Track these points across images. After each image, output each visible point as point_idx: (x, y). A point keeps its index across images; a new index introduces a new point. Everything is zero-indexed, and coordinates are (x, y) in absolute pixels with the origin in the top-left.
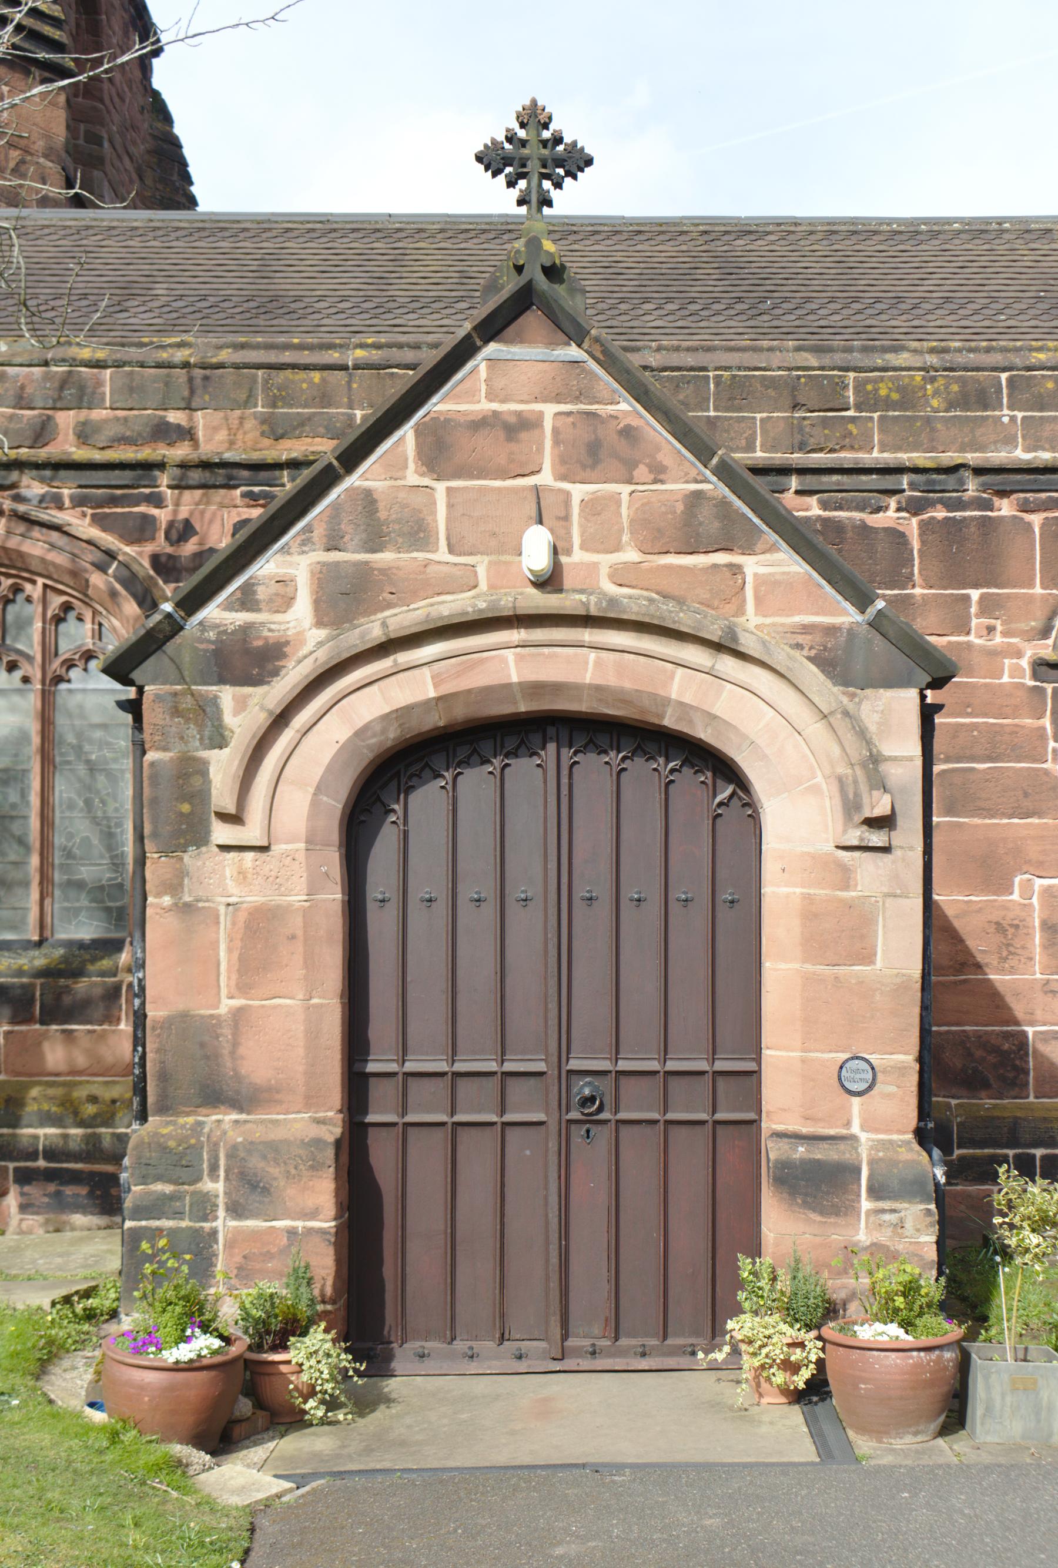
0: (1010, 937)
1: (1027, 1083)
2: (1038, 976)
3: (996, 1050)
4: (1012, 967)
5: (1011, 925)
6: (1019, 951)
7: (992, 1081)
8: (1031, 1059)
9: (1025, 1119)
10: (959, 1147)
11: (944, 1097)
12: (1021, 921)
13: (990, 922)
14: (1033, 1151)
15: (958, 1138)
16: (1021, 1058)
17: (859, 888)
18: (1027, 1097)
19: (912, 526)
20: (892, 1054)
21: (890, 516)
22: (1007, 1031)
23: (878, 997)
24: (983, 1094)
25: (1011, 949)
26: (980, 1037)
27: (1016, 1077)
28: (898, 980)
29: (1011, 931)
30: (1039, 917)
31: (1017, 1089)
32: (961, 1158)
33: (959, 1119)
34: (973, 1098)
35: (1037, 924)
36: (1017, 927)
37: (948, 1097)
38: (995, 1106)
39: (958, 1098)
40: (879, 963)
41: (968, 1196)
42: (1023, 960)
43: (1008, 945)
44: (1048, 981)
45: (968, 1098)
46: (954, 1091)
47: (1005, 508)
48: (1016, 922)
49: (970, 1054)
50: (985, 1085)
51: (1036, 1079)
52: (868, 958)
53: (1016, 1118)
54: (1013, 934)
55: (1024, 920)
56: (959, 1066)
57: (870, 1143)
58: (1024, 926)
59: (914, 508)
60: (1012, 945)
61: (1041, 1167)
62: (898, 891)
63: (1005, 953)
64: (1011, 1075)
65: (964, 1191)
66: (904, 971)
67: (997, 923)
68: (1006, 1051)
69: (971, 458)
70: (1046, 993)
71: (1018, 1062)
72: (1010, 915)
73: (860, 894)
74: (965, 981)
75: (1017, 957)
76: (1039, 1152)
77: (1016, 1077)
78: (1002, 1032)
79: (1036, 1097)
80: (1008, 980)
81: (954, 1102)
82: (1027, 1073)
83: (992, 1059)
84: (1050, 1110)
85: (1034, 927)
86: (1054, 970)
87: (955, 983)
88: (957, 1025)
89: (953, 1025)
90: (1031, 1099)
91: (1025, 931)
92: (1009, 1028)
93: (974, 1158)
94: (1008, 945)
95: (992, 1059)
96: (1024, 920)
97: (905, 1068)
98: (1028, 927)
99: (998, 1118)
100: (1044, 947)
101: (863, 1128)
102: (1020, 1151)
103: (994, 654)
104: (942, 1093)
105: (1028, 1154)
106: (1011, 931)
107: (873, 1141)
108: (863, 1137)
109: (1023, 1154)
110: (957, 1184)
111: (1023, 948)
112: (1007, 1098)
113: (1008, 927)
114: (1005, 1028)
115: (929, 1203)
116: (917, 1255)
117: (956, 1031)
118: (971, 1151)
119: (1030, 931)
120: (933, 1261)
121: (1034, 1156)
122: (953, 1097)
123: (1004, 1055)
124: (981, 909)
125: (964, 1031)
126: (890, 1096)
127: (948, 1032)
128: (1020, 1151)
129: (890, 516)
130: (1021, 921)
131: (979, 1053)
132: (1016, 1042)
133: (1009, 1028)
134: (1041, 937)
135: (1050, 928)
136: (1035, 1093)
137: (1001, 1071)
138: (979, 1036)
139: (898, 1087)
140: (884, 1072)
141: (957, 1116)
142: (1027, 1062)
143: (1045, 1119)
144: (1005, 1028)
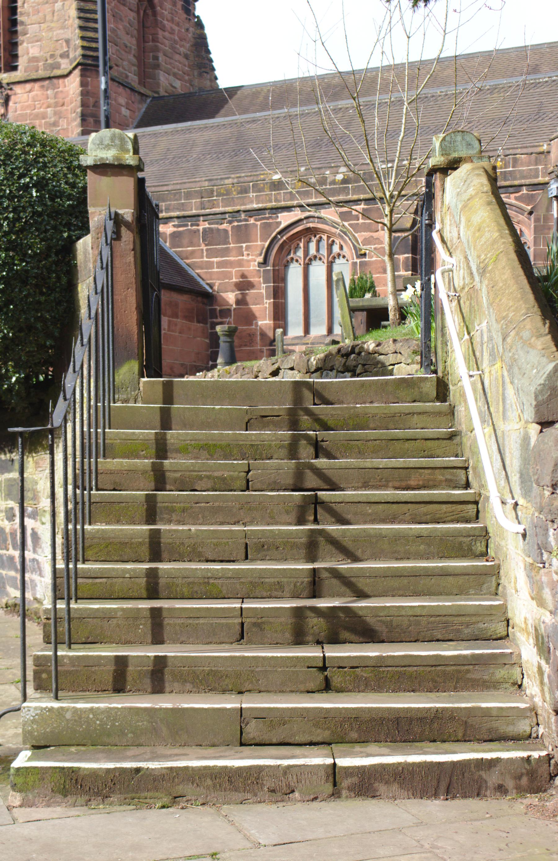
19: (229, 229)
21: (225, 226)
47: (252, 221)
59: (230, 222)
69: (243, 208)
103: (249, 261)
129: (225, 226)
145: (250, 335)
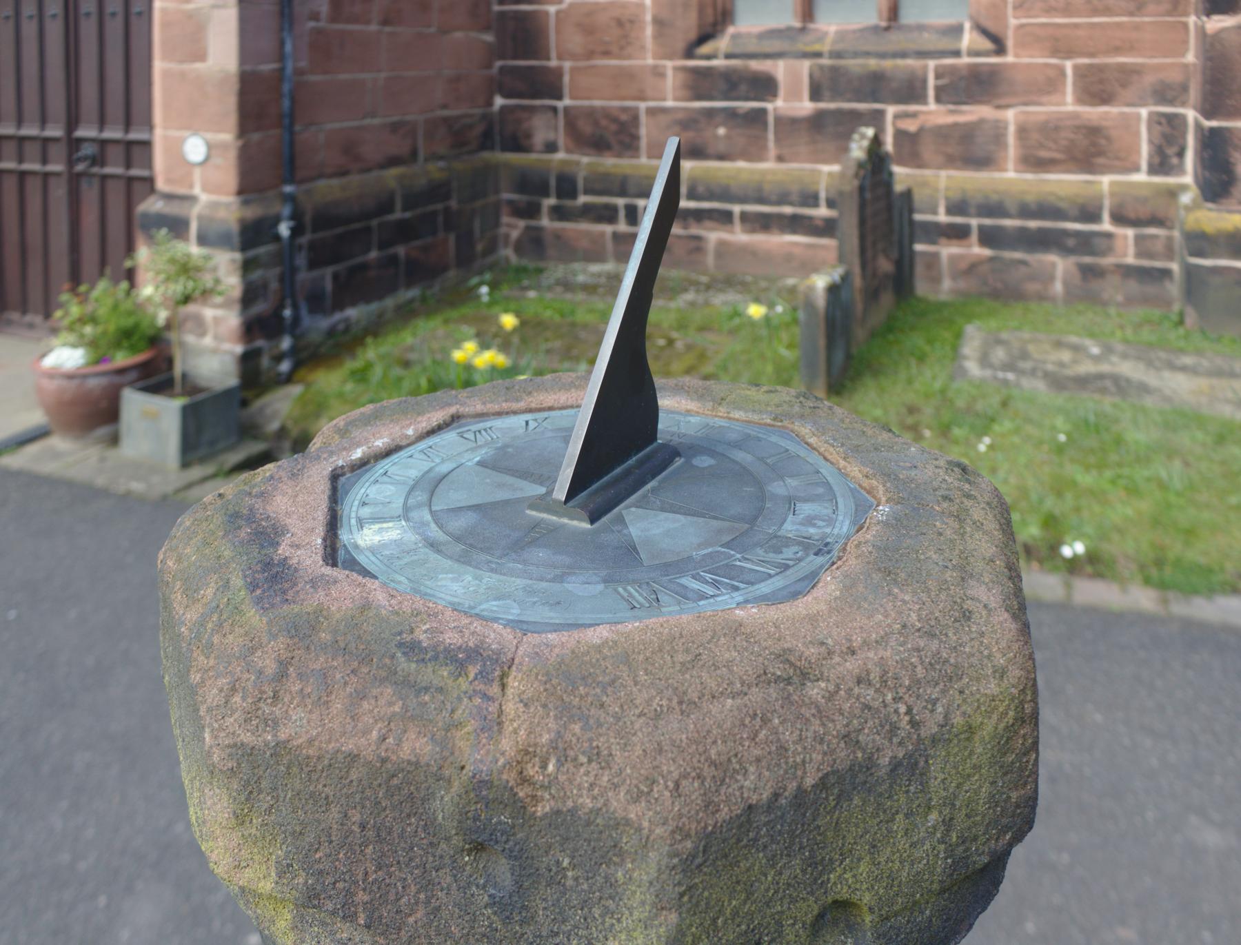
3: (615, 120)
52: (201, 56)
83: (613, 127)
95: (613, 127)
108: (204, 198)
138: (603, 109)
145: (620, 23)
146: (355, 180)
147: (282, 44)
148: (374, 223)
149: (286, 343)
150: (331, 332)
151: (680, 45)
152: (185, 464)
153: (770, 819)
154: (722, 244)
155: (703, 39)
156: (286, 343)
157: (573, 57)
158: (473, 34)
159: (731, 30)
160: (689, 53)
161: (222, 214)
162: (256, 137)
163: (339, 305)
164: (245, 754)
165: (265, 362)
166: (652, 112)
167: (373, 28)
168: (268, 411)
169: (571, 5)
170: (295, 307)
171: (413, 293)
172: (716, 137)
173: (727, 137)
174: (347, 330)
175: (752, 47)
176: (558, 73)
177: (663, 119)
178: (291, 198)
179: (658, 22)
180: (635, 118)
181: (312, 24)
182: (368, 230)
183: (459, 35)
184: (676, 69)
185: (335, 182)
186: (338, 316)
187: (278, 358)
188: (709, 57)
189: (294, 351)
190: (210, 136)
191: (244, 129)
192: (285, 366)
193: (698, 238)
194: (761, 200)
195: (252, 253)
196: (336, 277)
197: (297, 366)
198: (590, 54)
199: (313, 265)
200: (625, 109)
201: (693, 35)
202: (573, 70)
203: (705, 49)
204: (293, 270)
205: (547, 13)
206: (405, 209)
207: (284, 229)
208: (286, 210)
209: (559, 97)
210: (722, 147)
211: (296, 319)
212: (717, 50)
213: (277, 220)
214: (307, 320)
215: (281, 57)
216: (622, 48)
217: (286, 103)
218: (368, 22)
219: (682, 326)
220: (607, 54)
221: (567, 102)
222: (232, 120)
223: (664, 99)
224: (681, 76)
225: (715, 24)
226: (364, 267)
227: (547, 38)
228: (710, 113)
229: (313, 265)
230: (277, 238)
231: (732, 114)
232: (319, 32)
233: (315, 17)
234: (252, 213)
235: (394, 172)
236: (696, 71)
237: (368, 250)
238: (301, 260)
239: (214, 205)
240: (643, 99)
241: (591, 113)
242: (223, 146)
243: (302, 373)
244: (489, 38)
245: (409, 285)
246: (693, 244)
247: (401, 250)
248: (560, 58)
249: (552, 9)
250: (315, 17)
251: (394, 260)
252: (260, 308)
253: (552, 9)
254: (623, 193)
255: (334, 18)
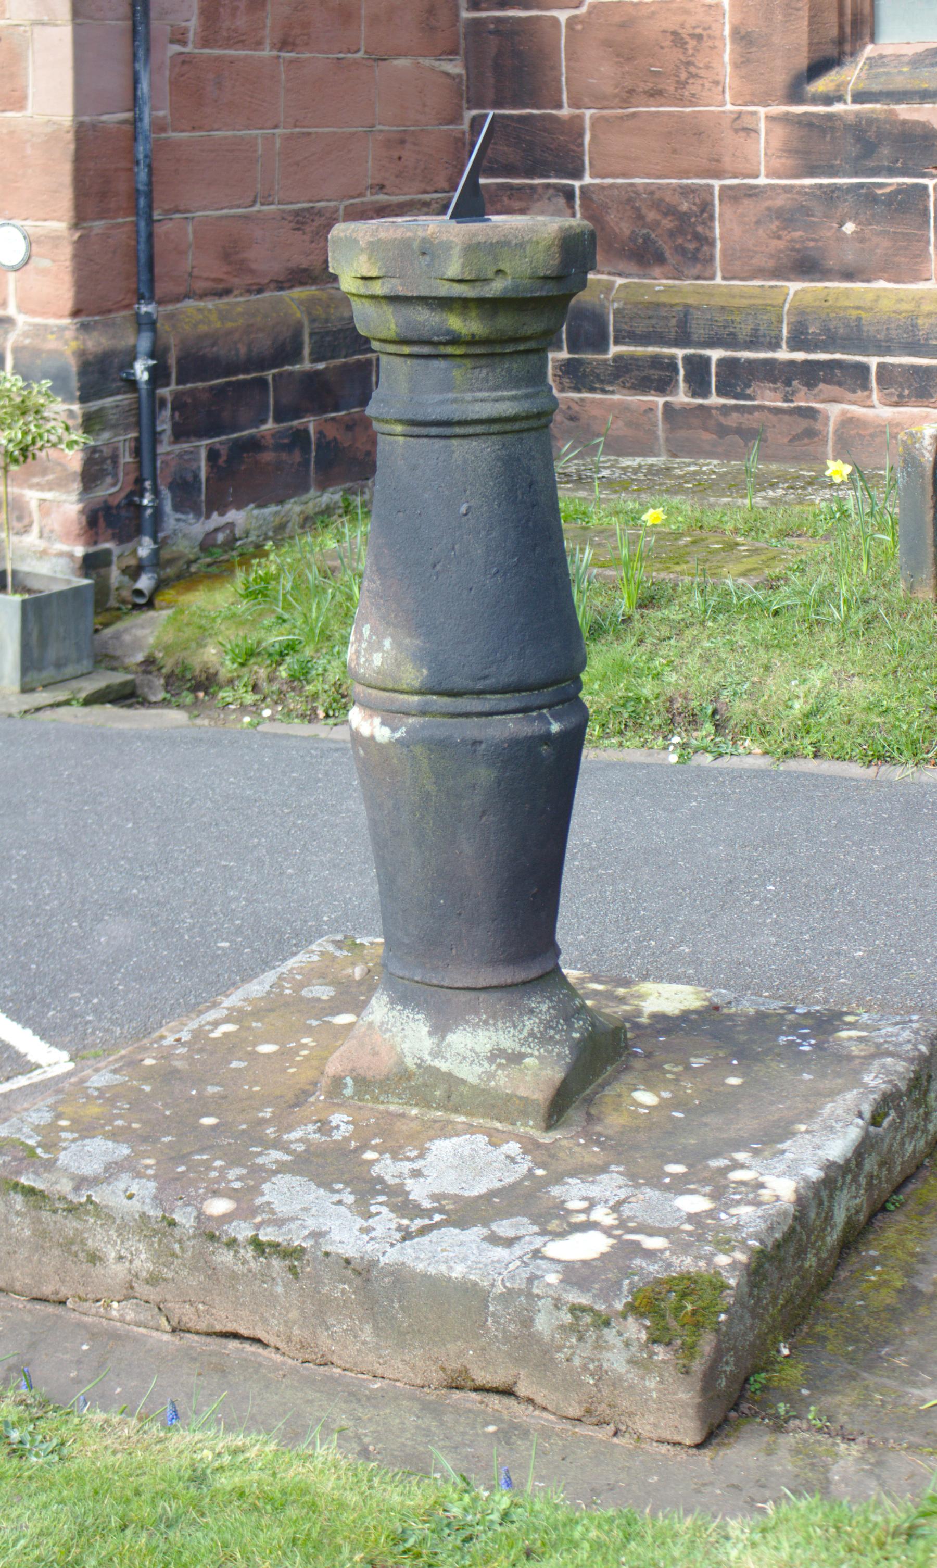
0: (690, 52)
1: (711, 259)
2: (729, 107)
3: (671, 211)
4: (693, 95)
5: (692, 36)
6: (702, 73)
7: (668, 254)
8: (717, 224)
9: (697, 308)
10: (616, 342)
11: (609, 274)
12: (705, 29)
13: (664, 32)
14: (708, 352)
15: (615, 330)
16: (704, 223)
17: (7, 15)
18: (712, 277)
20: (45, 220)
22: (687, 186)
23: (29, 151)
24: (657, 271)
25: (692, 69)
26: (652, 193)
27: (697, 250)
28: (49, 129)
29: (692, 43)
30: (730, 22)
31: (699, 266)
32: (618, 358)
33: (616, 305)
34: (644, 276)
35: (727, 32)
36: (699, 37)
37: (614, 274)
38: (668, 288)
39: (627, 276)
40: (29, 111)
41: (625, 408)
42: (707, 85)
43: (689, 64)
44: (739, 115)
45: (639, 277)
46: (622, 266)
48: (698, 31)
49: (640, 217)
50: (660, 259)
51: (723, 251)
52: (18, 103)
53: (687, 307)
54: (696, 49)
55: (709, 28)
56: (627, 232)
57: (26, 328)
58: (709, 37)
60: (693, 64)
61: (717, 375)
62: (46, 18)
63: (684, 76)
64: (691, 246)
65: (621, 403)
66: (54, 118)
67: (675, 33)
68: (685, 214)
70: (736, 131)
71: (699, 229)
72: (691, 21)
73: (8, 22)
74: (634, 115)
75: (700, 81)
76: (715, 355)
77: (697, 250)
78: (680, 186)
79: (724, 278)
80: (689, 114)
81: (620, 281)
82: (712, 244)
83: (668, 223)
84: (733, 297)
85: (723, 38)
86: (748, 98)
87: (621, 118)
88: (624, 175)
89: (617, 177)
90: (719, 280)
91: (710, 43)
92: (689, 181)
93: (633, 358)
94: (689, 64)
95: (668, 223)
96: (709, 28)
97: (58, 238)
98: (715, 38)
99: (664, 305)
100: (736, 66)
101: (21, 309)
102: (692, 351)
104: (607, 269)
105: (701, 357)
106: (692, 43)
107: (30, 325)
108: (22, 320)
109: (694, 355)
110: (613, 392)
111: (707, 67)
112: (688, 278)
113: (688, 39)
114: (685, 181)
115: (72, 403)
116: (60, 464)
117: (622, 185)
118: (632, 349)
119: (717, 43)
120: (75, 473)
121: (708, 360)
122: (620, 275)
123: (682, 218)
124: (653, 13)
125: (632, 185)
126: (44, 272)
127: (612, 186)
128: (692, 351)
130: (705, 29)
131: (651, 215)
132: (697, 201)
133: (689, 181)
134: (732, 51)
135: (742, 38)
136: (722, 271)
137: (680, 241)
138: (651, 191)
139: (54, 261)
140: (38, 242)
141: (613, 301)
142: (712, 229)
143: (723, 309)
144: (685, 181)
145: (677, 39)
146: (238, 302)
147: (136, 81)
148: (270, 374)
149: (145, 548)
150: (206, 545)
151: (781, 78)
152: (26, 689)
153: (600, 570)
154: (848, 422)
155: (817, 68)
156: (145, 548)
157: (600, 101)
158: (427, 62)
159: (869, 50)
160: (795, 94)
161: (52, 343)
162: (98, 226)
163: (217, 504)
164: (370, 243)
165: (115, 575)
166: (730, 195)
167: (267, 53)
168: (127, 638)
169: (593, 7)
170: (156, 492)
171: (332, 496)
172: (841, 238)
173: (859, 237)
174: (230, 543)
175: (899, 83)
176: (574, 129)
177: (751, 209)
178: (150, 324)
179: (742, 37)
180: (706, 207)
181: (177, 48)
182: (262, 382)
183: (402, 63)
184: (770, 118)
185: (210, 304)
186: (216, 520)
187: (134, 572)
188: (828, 100)
189: (156, 562)
190: (29, 225)
191: (80, 218)
192: (145, 583)
193: (810, 413)
194: (913, 348)
195: (95, 405)
196: (213, 455)
197: (160, 585)
198: (628, 96)
199: (180, 434)
200: (686, 191)
201: (802, 61)
202: (595, 121)
203: (822, 85)
204: (155, 437)
205: (556, 21)
206: (315, 360)
207: (141, 371)
208: (144, 343)
209: (577, 173)
210: (850, 257)
211: (158, 513)
212: (843, 85)
213: (132, 356)
214: (171, 519)
215: (135, 102)
216: (682, 84)
217: (143, 175)
218: (259, 44)
219: (753, 529)
220: (655, 94)
221: (587, 180)
222: (65, 200)
223: (756, 176)
224: (780, 131)
225: (840, 41)
226: (254, 445)
227: (556, 67)
228: (830, 195)
229: (180, 434)
230: (132, 384)
231: (868, 197)
232: (185, 60)
233: (179, 38)
234: (97, 342)
235: (299, 293)
236: (807, 124)
237: (264, 421)
238: (164, 424)
239: (40, 331)
240: (718, 175)
241: (630, 198)
242: (54, 240)
243: (169, 594)
244: (455, 67)
245: (323, 486)
246: (804, 423)
247: (311, 424)
248: (574, 104)
249: (563, 16)
250: (179, 38)
251: (301, 437)
252: (106, 491)
253: (563, 16)
254: (683, 340)
255: (206, 42)
